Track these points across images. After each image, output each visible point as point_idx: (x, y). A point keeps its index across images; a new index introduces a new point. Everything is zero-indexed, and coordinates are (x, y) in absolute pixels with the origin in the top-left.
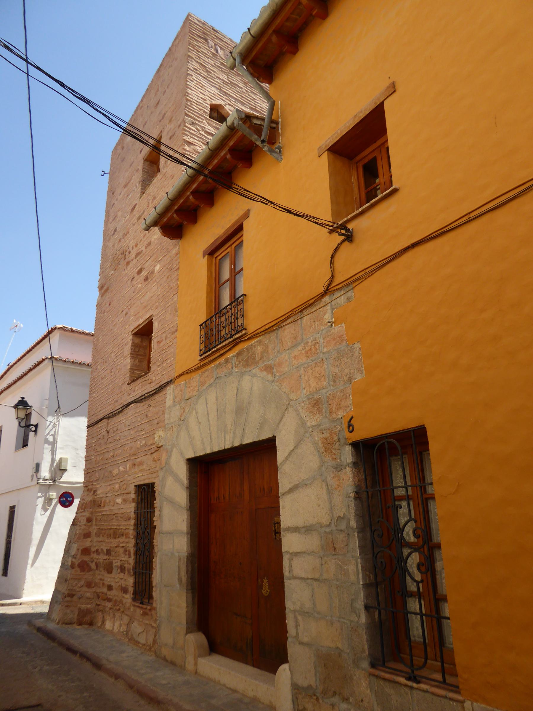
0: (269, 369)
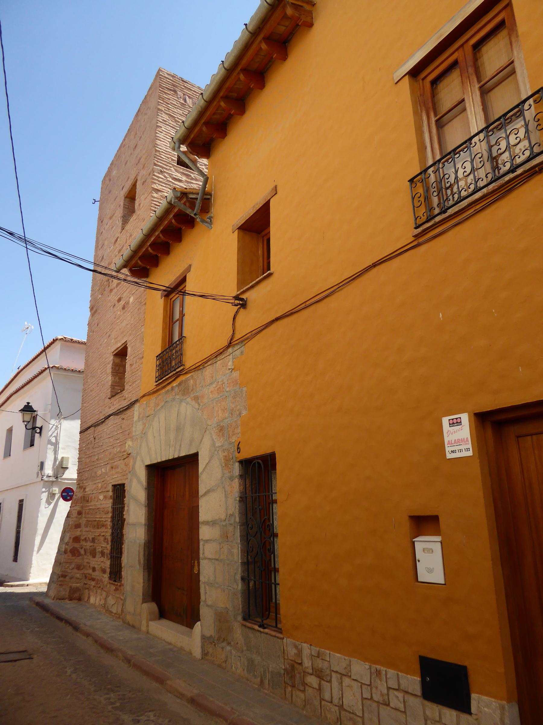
0: (196, 399)
